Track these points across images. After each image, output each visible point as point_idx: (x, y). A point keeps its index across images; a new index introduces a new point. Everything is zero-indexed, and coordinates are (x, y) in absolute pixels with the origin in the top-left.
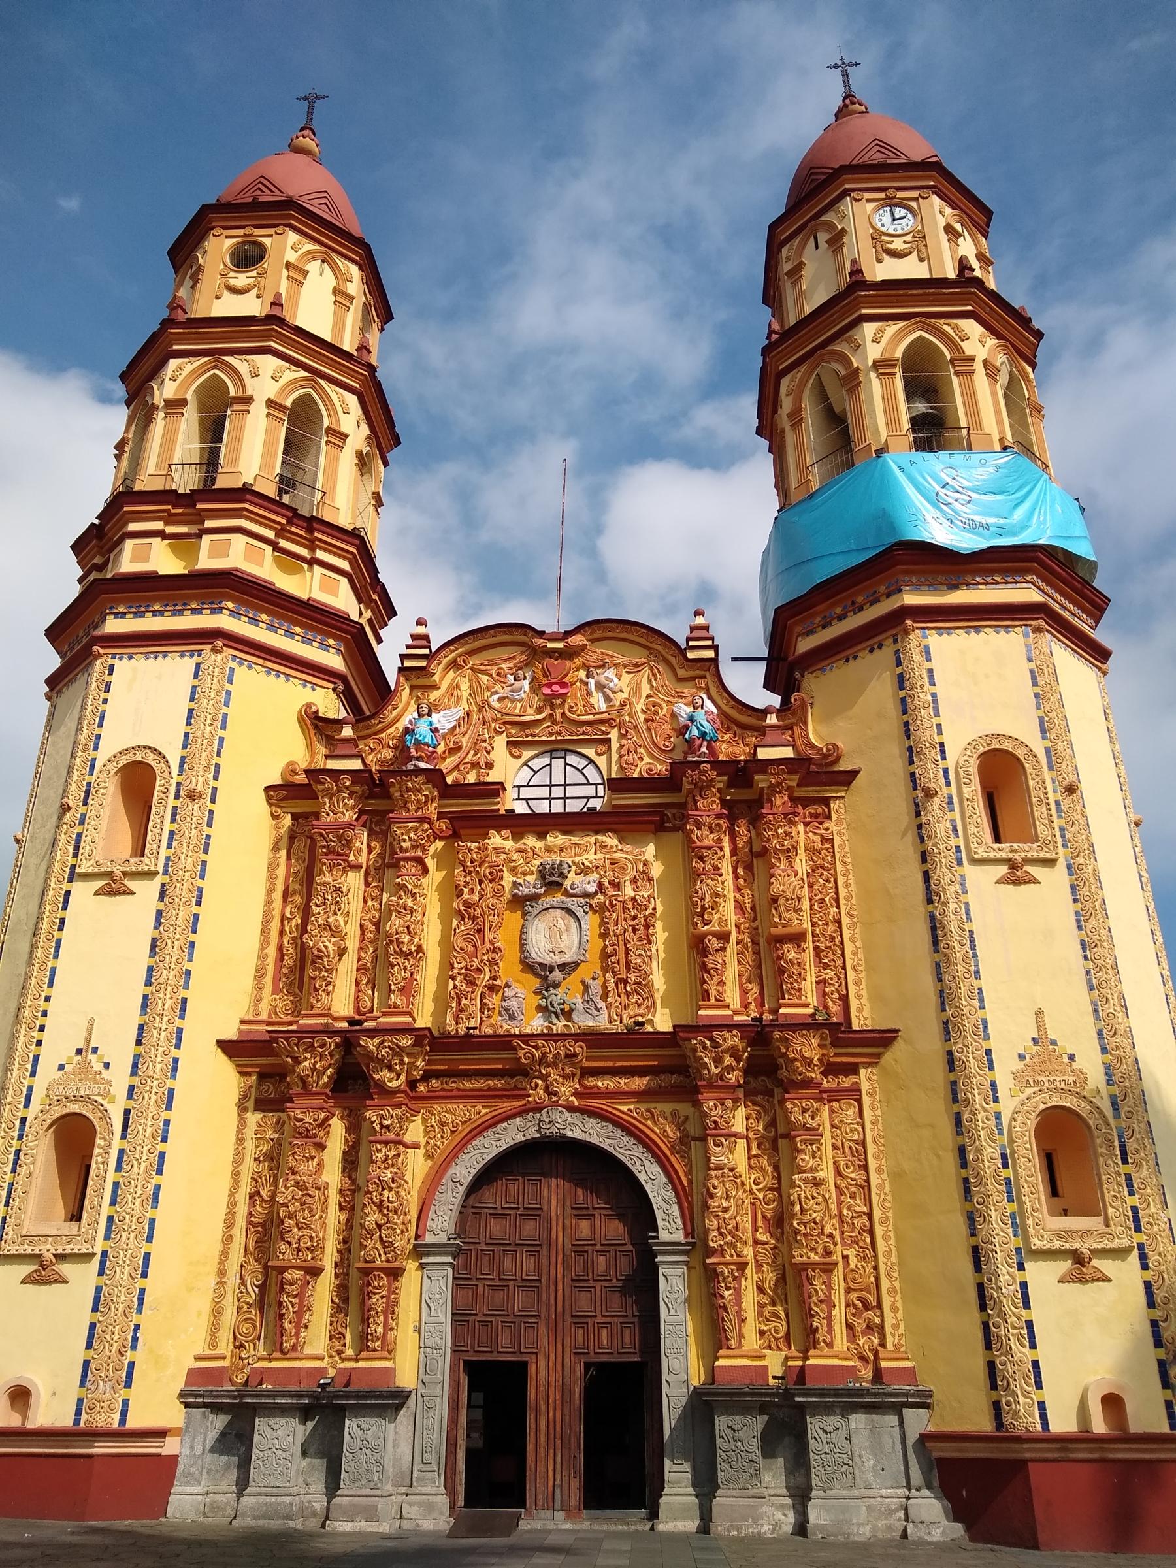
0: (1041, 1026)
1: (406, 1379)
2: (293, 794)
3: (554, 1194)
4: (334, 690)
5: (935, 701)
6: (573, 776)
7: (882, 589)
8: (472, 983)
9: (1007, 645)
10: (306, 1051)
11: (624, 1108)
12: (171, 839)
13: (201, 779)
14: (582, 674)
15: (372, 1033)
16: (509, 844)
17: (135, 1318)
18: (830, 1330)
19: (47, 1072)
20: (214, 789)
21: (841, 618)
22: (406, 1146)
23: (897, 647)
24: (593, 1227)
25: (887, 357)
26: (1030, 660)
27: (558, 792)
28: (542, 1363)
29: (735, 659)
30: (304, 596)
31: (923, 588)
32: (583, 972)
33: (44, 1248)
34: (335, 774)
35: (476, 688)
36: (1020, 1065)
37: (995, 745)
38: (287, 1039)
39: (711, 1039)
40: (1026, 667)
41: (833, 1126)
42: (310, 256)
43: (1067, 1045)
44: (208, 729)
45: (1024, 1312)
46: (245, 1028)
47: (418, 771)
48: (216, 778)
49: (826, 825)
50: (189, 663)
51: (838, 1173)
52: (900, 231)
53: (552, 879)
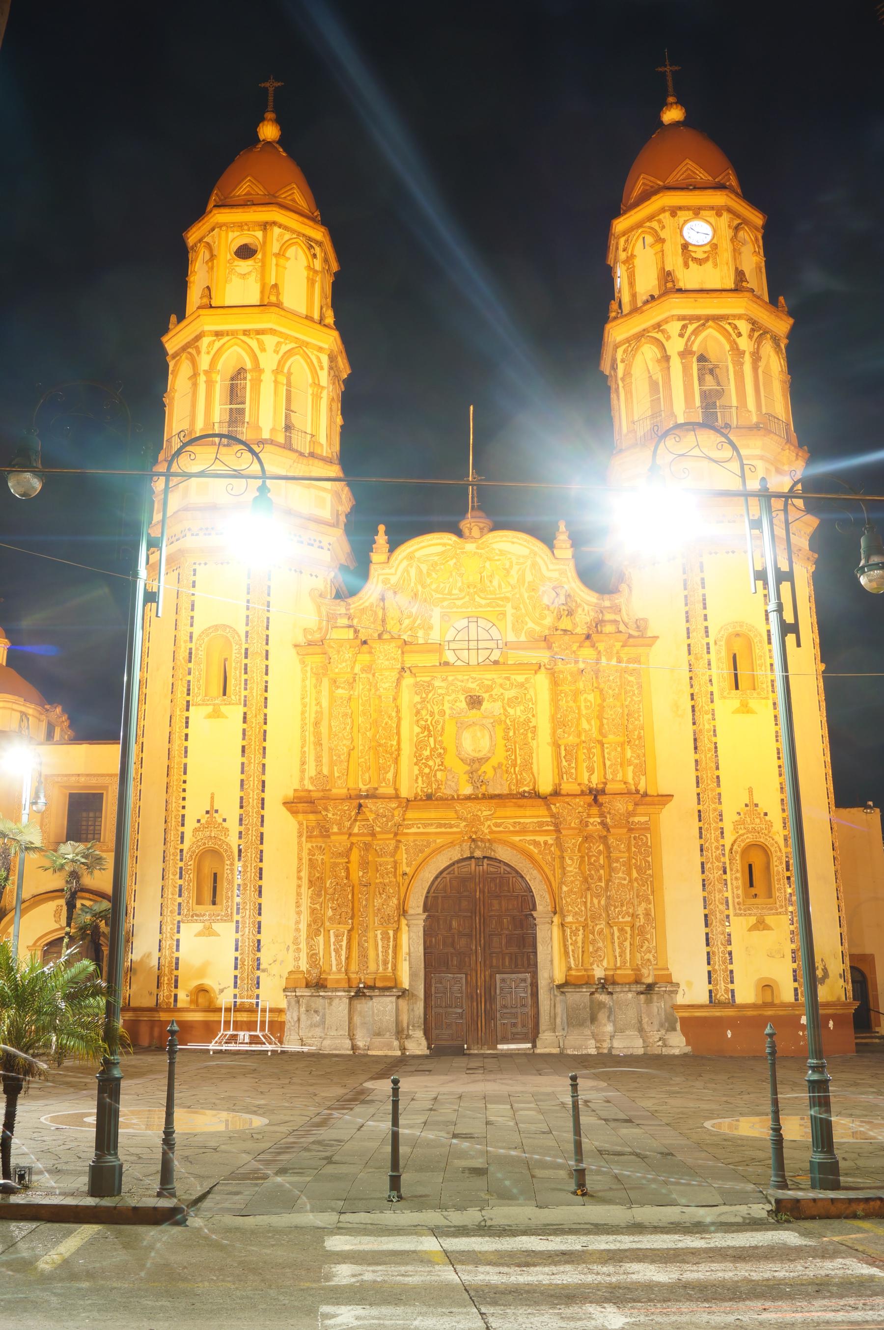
12: (246, 684)
19: (190, 825)
36: (737, 818)
43: (763, 807)
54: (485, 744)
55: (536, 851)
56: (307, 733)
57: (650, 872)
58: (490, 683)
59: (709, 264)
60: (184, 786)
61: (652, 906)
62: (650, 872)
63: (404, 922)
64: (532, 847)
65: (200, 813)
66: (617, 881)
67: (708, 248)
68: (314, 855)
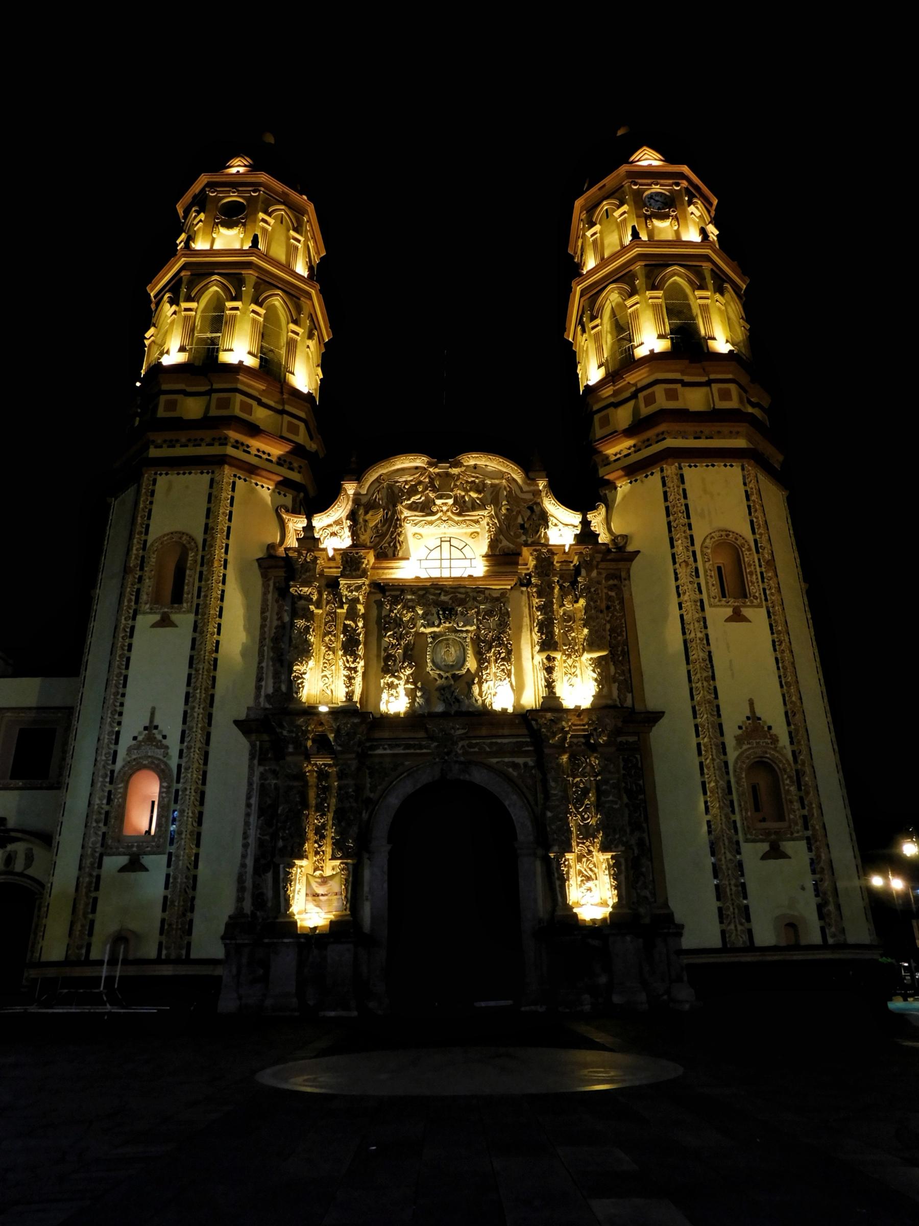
31: (626, 596)
36: (740, 732)
50: (207, 478)
55: (515, 774)
56: (266, 648)
57: (641, 797)
58: (463, 596)
61: (645, 835)
62: (641, 797)
63: (366, 855)
64: (510, 770)
66: (607, 805)
68: (266, 780)
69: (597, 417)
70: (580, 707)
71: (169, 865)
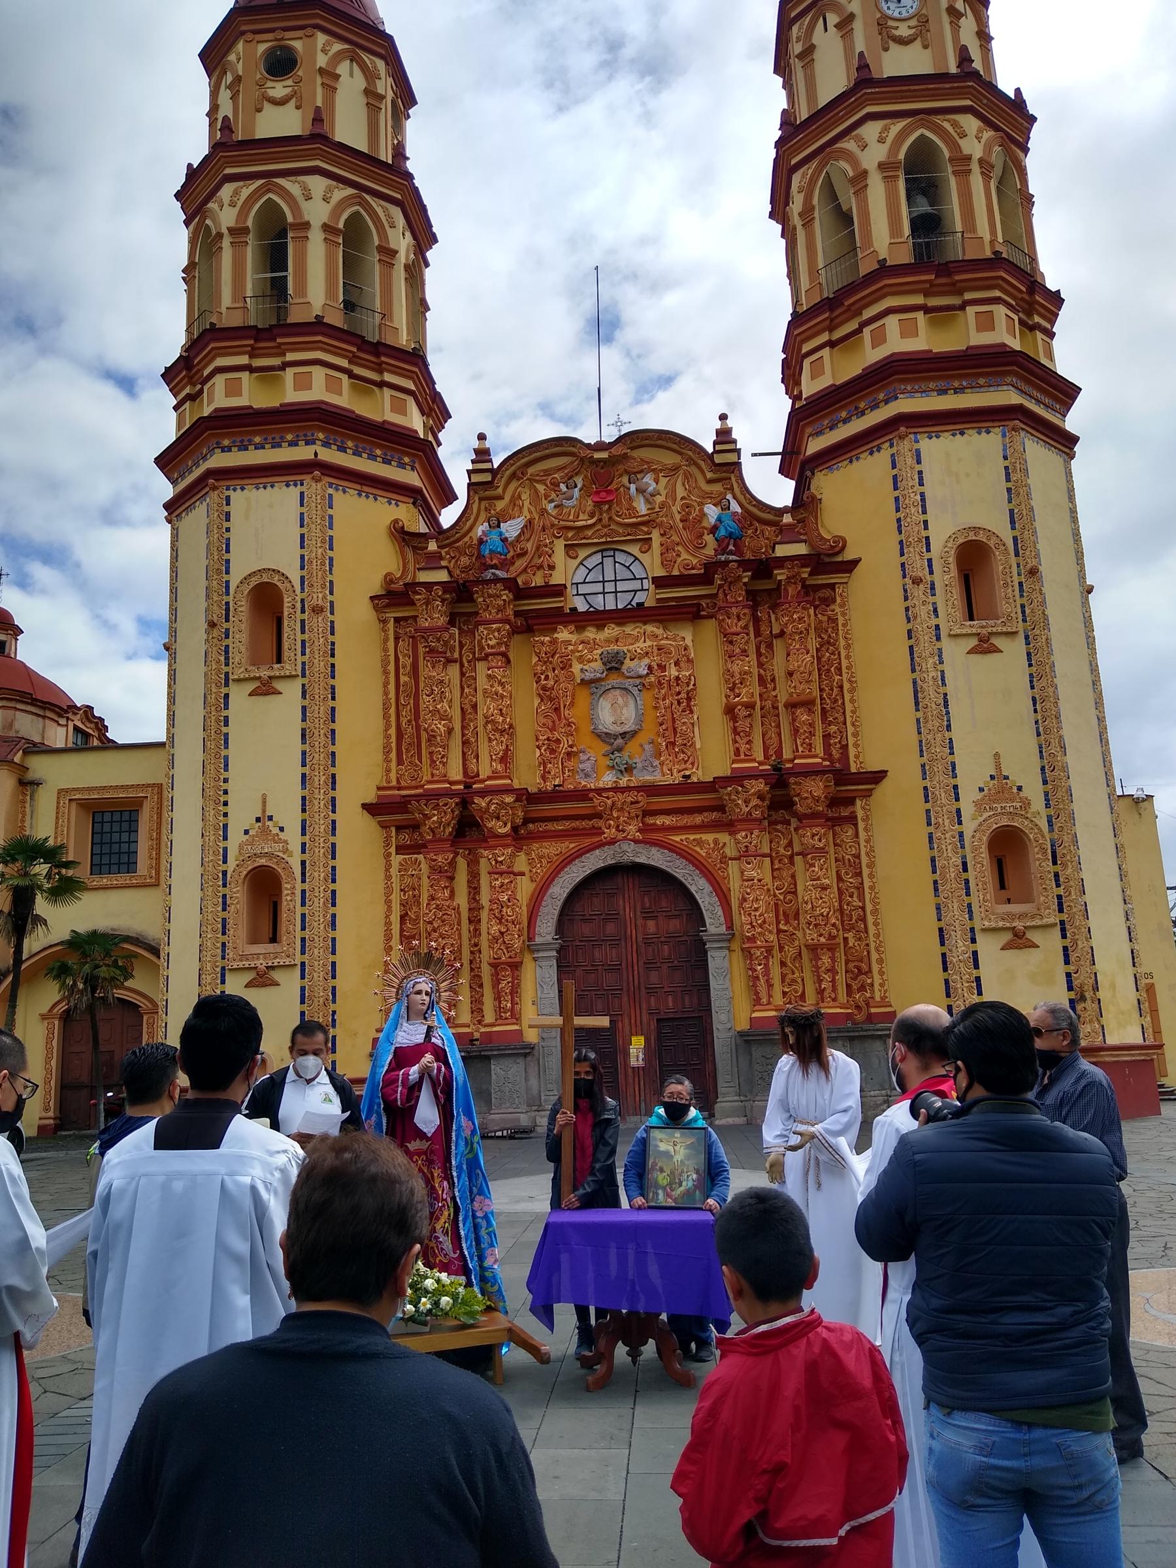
0: (998, 766)
1: (531, 1036)
2: (394, 598)
3: (628, 903)
4: (414, 504)
5: (923, 500)
6: (622, 573)
7: (881, 396)
8: (553, 751)
9: (986, 445)
10: (433, 809)
11: (677, 838)
13: (320, 595)
14: (625, 480)
15: (483, 793)
16: (574, 638)
17: (332, 1007)
18: (834, 989)
20: (332, 603)
21: (845, 421)
22: (515, 874)
23: (894, 450)
24: (657, 924)
25: (892, 160)
26: (1005, 458)
27: (610, 587)
28: (626, 1021)
29: (754, 455)
30: (378, 418)
31: (916, 395)
32: (642, 738)
33: (258, 963)
34: (429, 586)
35: (536, 497)
36: (979, 796)
37: (972, 537)
38: (418, 801)
39: (742, 786)
40: (1002, 464)
41: (835, 845)
42: (338, 58)
43: (1017, 778)
44: (320, 551)
45: (975, 971)
46: (380, 793)
47: (496, 580)
48: (331, 593)
49: (832, 607)
50: (294, 492)
51: (840, 879)
52: (905, 15)
53: (614, 664)
54: (590, 502)
59: (918, 44)
60: (225, 786)
65: (248, 821)
67: (913, 22)
69: (806, 363)
70: (810, 1287)
71: (303, 977)
